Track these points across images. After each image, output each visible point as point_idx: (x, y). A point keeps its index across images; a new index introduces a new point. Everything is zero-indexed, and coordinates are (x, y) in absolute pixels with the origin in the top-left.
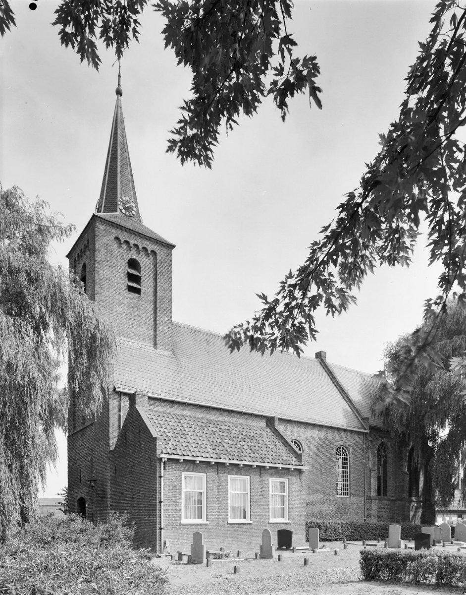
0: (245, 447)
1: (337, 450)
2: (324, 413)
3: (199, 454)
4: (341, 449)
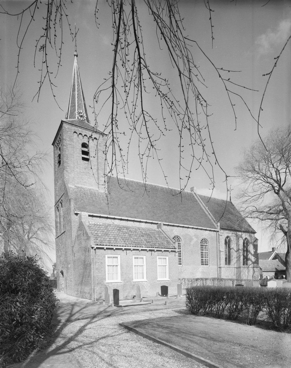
0: (143, 240)
1: (201, 241)
2: (157, 235)
3: (116, 244)
4: (204, 240)
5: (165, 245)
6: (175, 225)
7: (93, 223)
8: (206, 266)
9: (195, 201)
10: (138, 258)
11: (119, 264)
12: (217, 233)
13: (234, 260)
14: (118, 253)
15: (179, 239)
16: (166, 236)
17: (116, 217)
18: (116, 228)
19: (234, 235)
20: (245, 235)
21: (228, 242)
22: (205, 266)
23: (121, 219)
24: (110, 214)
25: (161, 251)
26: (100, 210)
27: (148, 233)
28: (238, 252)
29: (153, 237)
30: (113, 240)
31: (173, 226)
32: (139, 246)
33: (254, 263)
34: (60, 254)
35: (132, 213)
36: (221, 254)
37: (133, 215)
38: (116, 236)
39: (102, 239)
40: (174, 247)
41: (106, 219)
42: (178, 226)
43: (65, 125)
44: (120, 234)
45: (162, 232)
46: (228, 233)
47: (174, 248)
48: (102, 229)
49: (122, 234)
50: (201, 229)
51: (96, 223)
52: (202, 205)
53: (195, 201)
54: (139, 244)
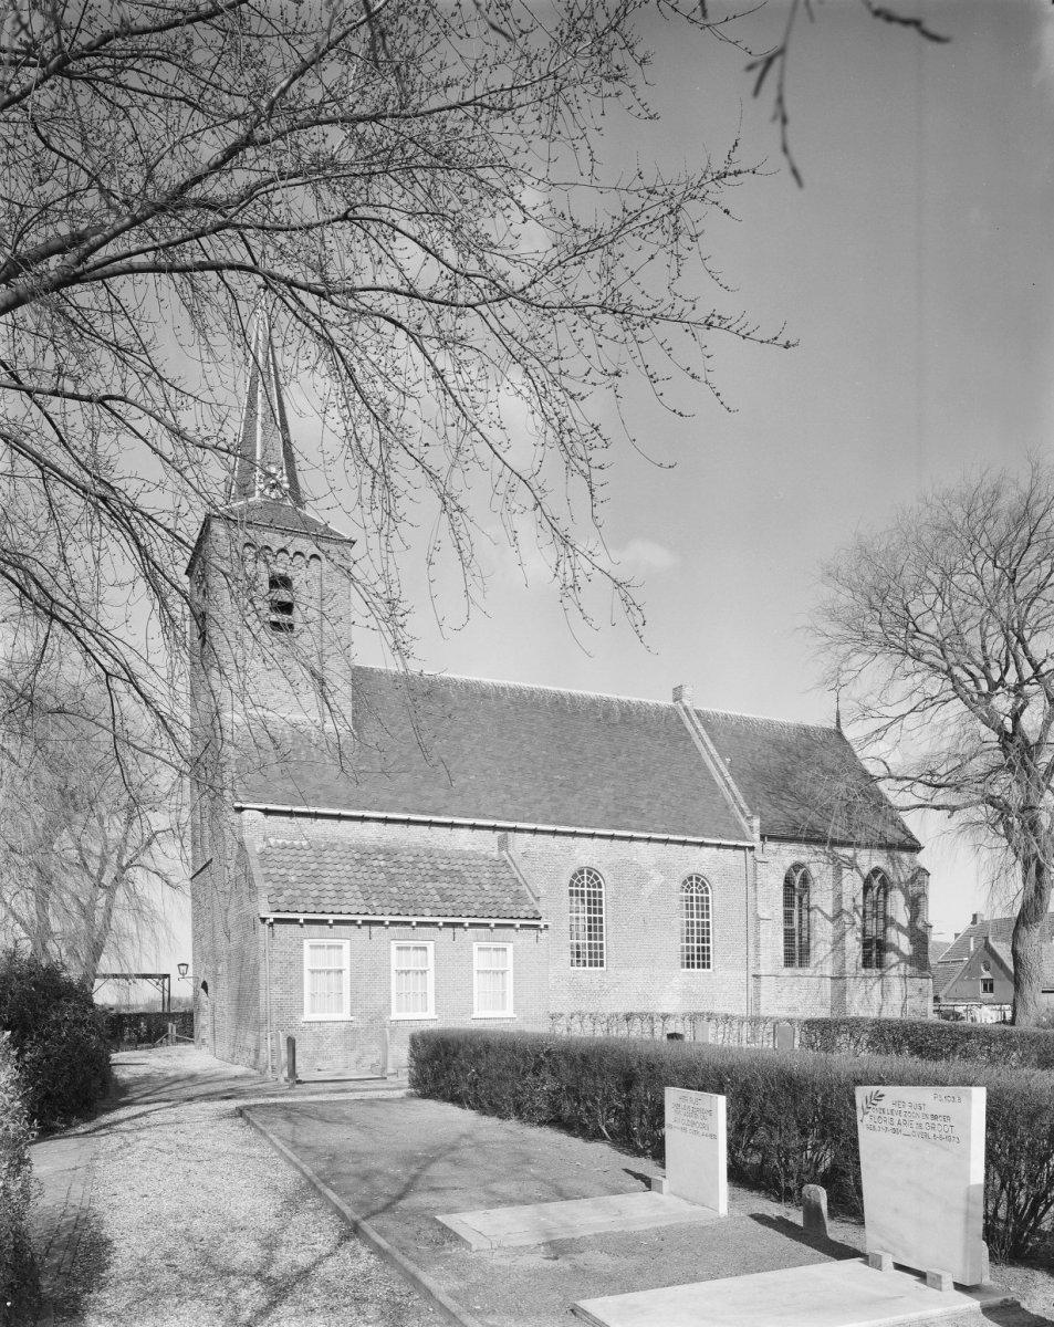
3: (337, 909)
5: (505, 907)
6: (579, 830)
7: (280, 842)
8: (701, 970)
9: (682, 738)
10: (408, 948)
11: (346, 965)
12: (750, 854)
13: (821, 949)
14: (343, 935)
15: (597, 878)
16: (517, 875)
17: (367, 814)
18: (349, 855)
19: (823, 858)
20: (870, 860)
21: (796, 888)
22: (696, 970)
23: (386, 821)
24: (347, 806)
25: (487, 925)
26: (319, 792)
27: (456, 867)
28: (836, 922)
29: (470, 880)
30: (332, 894)
31: (574, 834)
32: (411, 912)
33: (910, 960)
34: (199, 929)
35: (428, 798)
36: (763, 927)
37: (430, 803)
38: (345, 881)
39: (298, 893)
40: (536, 912)
41: (336, 822)
42: (592, 836)
43: (218, 528)
44: (359, 875)
45: (509, 862)
46: (798, 852)
47: (532, 915)
48: (304, 859)
49: (366, 876)
50: (684, 843)
51: (288, 843)
52: (708, 751)
53: (682, 738)
54: (414, 904)
